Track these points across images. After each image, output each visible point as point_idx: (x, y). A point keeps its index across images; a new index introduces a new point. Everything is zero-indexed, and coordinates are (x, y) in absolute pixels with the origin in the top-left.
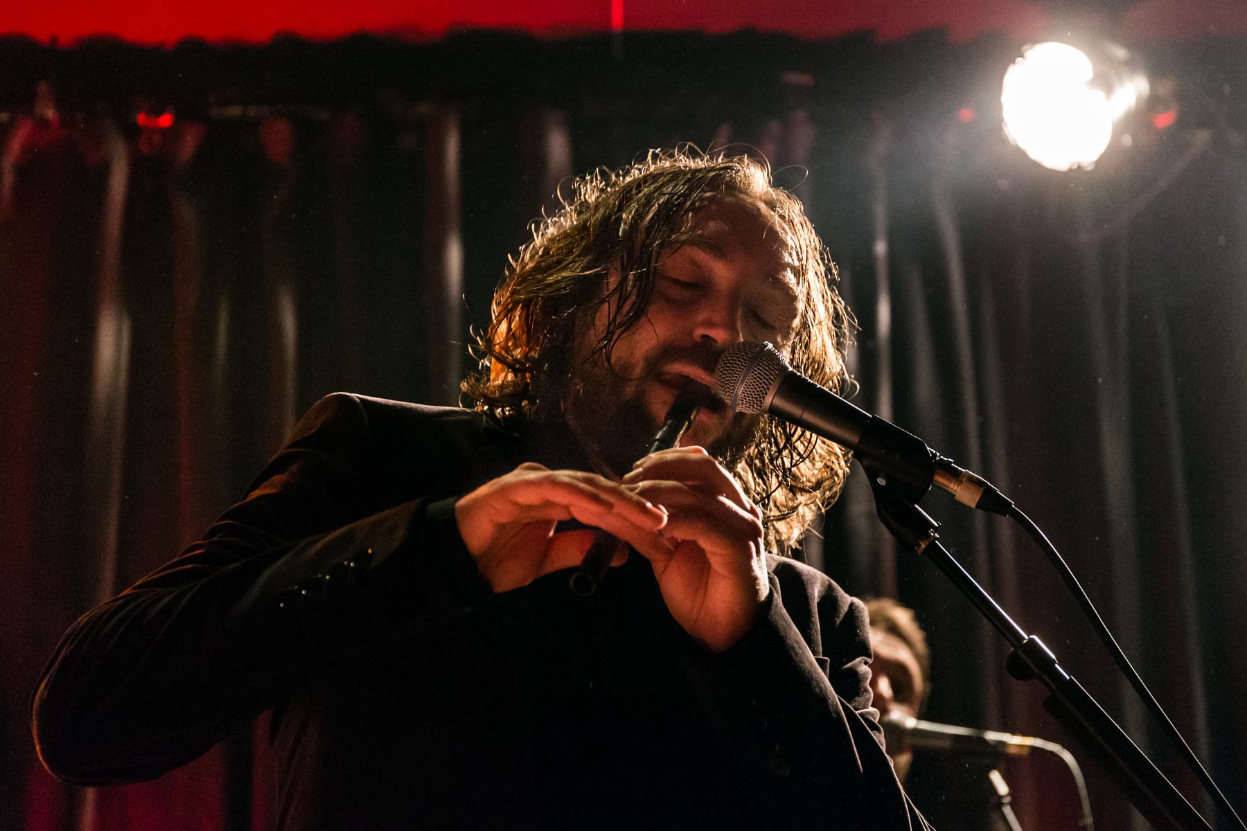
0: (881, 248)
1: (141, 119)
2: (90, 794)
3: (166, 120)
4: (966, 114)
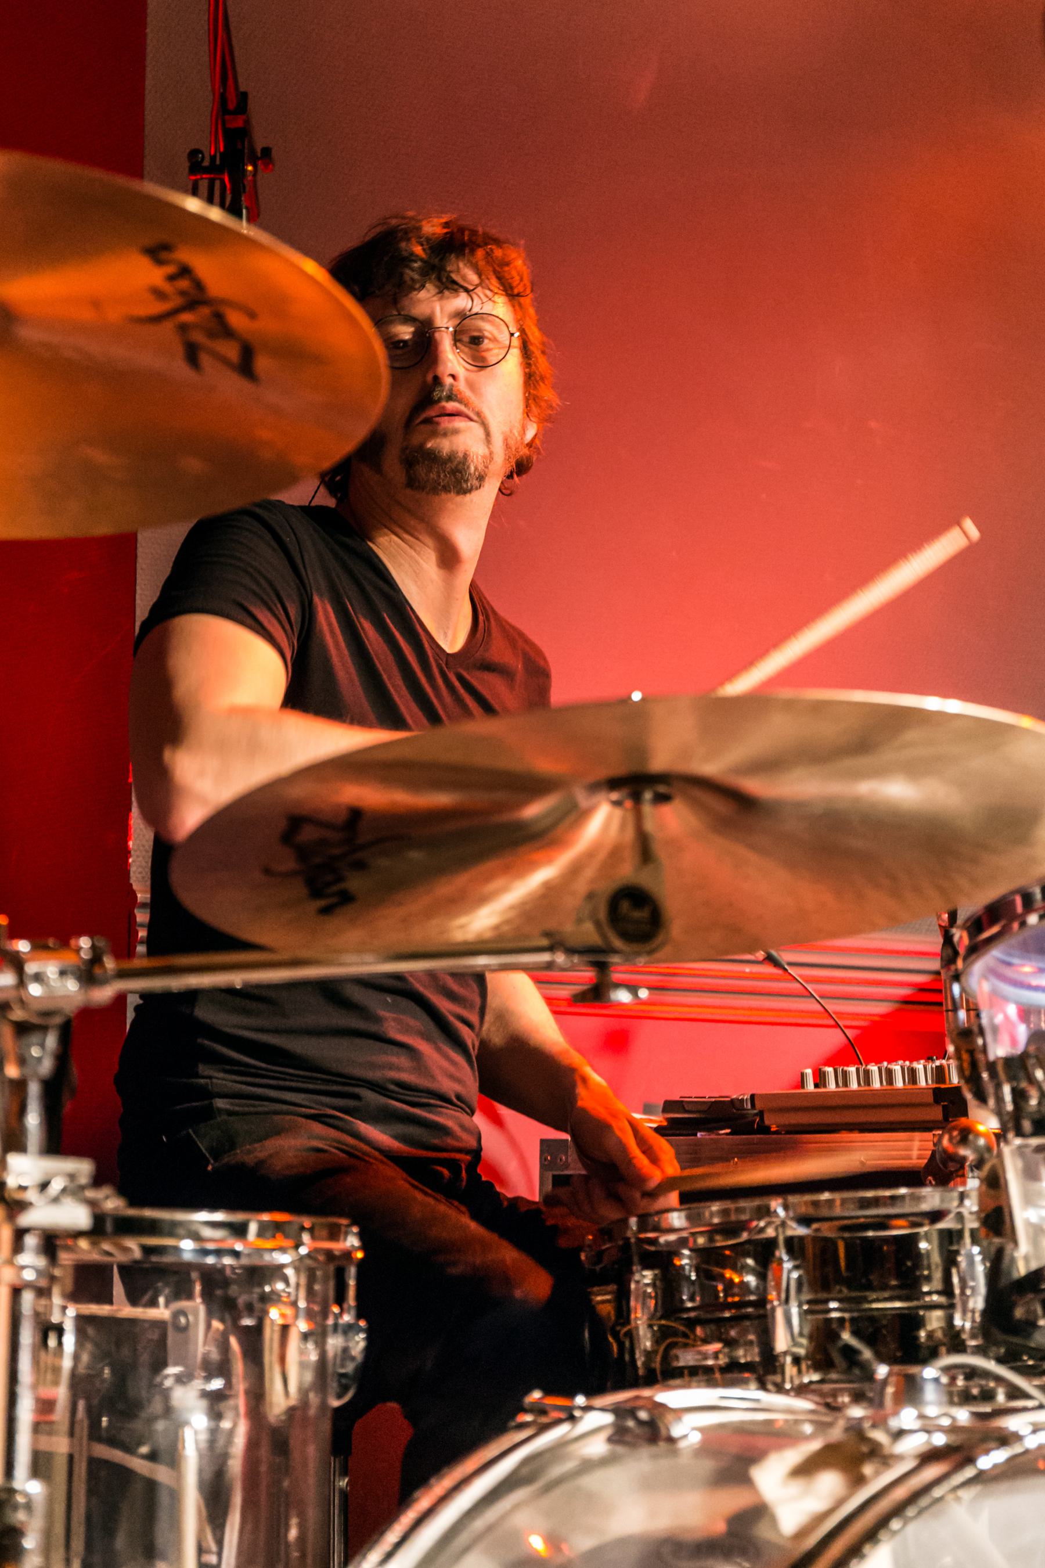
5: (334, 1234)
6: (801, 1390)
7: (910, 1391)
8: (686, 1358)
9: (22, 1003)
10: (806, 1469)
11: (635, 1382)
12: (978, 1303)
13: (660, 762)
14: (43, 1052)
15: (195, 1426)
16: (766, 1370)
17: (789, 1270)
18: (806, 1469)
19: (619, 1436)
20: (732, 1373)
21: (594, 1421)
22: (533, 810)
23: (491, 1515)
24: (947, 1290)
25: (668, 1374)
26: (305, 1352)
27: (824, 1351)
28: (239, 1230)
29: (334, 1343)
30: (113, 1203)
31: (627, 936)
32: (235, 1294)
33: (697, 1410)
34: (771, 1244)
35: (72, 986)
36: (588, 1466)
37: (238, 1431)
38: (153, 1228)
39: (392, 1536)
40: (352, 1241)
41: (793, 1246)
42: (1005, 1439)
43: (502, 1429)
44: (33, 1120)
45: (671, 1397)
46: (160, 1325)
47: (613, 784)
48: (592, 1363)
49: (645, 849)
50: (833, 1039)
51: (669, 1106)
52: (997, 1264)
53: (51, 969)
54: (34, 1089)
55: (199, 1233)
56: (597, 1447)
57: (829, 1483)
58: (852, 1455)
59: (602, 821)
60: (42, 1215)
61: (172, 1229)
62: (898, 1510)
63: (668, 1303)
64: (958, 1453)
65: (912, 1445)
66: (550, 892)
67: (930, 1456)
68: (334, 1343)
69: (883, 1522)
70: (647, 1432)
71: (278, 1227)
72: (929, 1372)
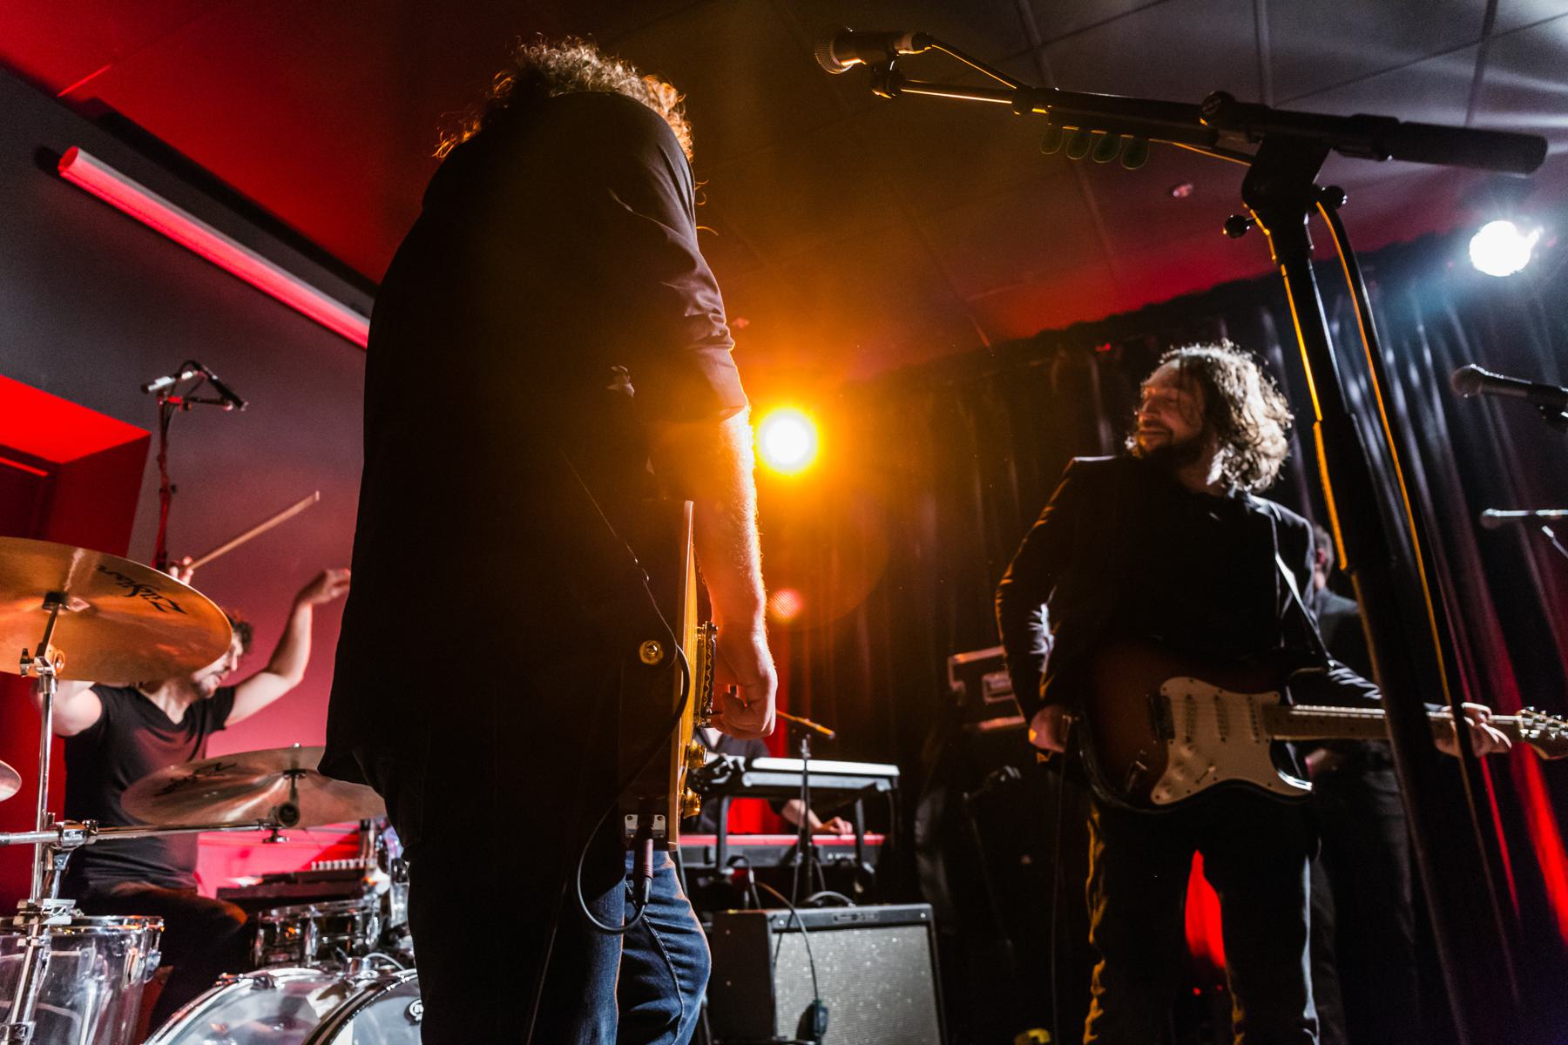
0: (1421, 329)
1: (1098, 349)
2: (892, 770)
3: (1108, 347)
4: (1450, 264)
5: (156, 922)
6: (313, 967)
7: (358, 965)
8: (273, 959)
9: (60, 843)
10: (323, 997)
11: (258, 968)
12: (375, 936)
13: (301, 767)
14: (62, 863)
15: (93, 992)
16: (301, 962)
17: (314, 928)
18: (323, 997)
19: (255, 987)
20: (289, 963)
21: (246, 982)
22: (257, 780)
23: (204, 1018)
24: (364, 932)
25: (266, 964)
26: (140, 961)
27: (323, 954)
28: (121, 922)
29: (149, 960)
30: (79, 914)
31: (285, 821)
32: (112, 948)
33: (284, 976)
34: (308, 920)
35: (80, 837)
36: (241, 998)
37: (107, 994)
38: (90, 923)
39: (165, 1029)
40: (160, 924)
41: (317, 920)
42: (395, 980)
43: (210, 987)
44: (55, 886)
45: (274, 972)
46: (77, 958)
47: (286, 772)
48: (243, 964)
49: (294, 793)
50: (316, 853)
51: (264, 876)
52: (385, 924)
53: (73, 831)
54: (58, 874)
55: (107, 923)
56: (247, 991)
57: (333, 1001)
58: (341, 989)
59: (281, 785)
60: (54, 920)
61: (98, 923)
62: (359, 1007)
63: (269, 940)
64: (378, 986)
65: (365, 983)
66: (259, 807)
67: (368, 988)
68: (149, 960)
69: (354, 1011)
70: (265, 984)
71: (137, 921)
72: (365, 960)
